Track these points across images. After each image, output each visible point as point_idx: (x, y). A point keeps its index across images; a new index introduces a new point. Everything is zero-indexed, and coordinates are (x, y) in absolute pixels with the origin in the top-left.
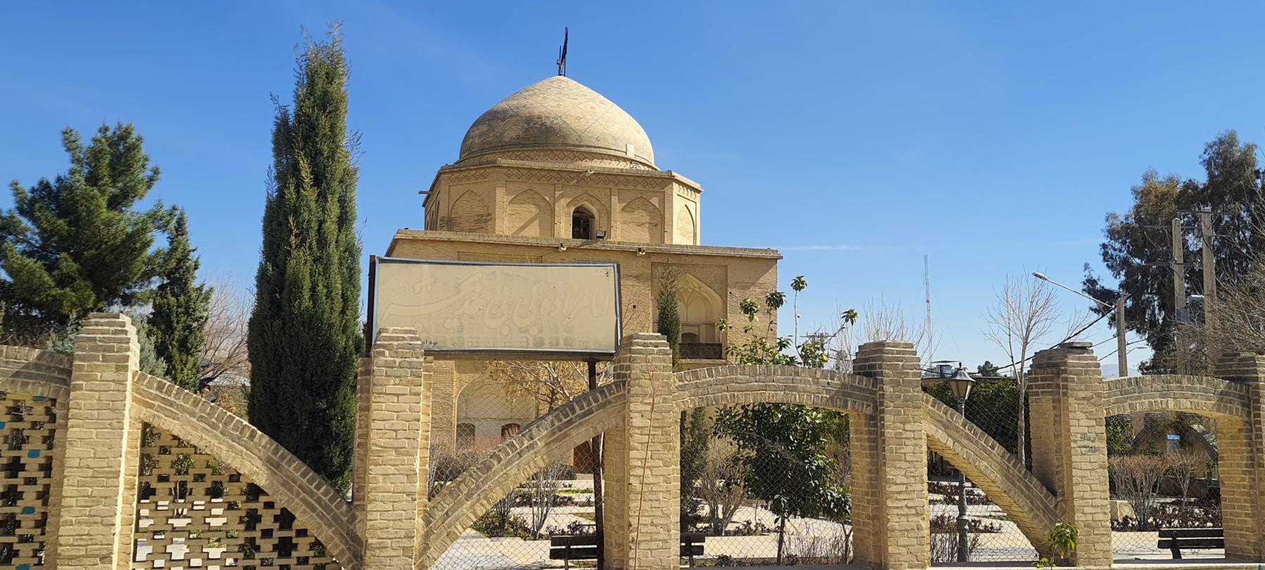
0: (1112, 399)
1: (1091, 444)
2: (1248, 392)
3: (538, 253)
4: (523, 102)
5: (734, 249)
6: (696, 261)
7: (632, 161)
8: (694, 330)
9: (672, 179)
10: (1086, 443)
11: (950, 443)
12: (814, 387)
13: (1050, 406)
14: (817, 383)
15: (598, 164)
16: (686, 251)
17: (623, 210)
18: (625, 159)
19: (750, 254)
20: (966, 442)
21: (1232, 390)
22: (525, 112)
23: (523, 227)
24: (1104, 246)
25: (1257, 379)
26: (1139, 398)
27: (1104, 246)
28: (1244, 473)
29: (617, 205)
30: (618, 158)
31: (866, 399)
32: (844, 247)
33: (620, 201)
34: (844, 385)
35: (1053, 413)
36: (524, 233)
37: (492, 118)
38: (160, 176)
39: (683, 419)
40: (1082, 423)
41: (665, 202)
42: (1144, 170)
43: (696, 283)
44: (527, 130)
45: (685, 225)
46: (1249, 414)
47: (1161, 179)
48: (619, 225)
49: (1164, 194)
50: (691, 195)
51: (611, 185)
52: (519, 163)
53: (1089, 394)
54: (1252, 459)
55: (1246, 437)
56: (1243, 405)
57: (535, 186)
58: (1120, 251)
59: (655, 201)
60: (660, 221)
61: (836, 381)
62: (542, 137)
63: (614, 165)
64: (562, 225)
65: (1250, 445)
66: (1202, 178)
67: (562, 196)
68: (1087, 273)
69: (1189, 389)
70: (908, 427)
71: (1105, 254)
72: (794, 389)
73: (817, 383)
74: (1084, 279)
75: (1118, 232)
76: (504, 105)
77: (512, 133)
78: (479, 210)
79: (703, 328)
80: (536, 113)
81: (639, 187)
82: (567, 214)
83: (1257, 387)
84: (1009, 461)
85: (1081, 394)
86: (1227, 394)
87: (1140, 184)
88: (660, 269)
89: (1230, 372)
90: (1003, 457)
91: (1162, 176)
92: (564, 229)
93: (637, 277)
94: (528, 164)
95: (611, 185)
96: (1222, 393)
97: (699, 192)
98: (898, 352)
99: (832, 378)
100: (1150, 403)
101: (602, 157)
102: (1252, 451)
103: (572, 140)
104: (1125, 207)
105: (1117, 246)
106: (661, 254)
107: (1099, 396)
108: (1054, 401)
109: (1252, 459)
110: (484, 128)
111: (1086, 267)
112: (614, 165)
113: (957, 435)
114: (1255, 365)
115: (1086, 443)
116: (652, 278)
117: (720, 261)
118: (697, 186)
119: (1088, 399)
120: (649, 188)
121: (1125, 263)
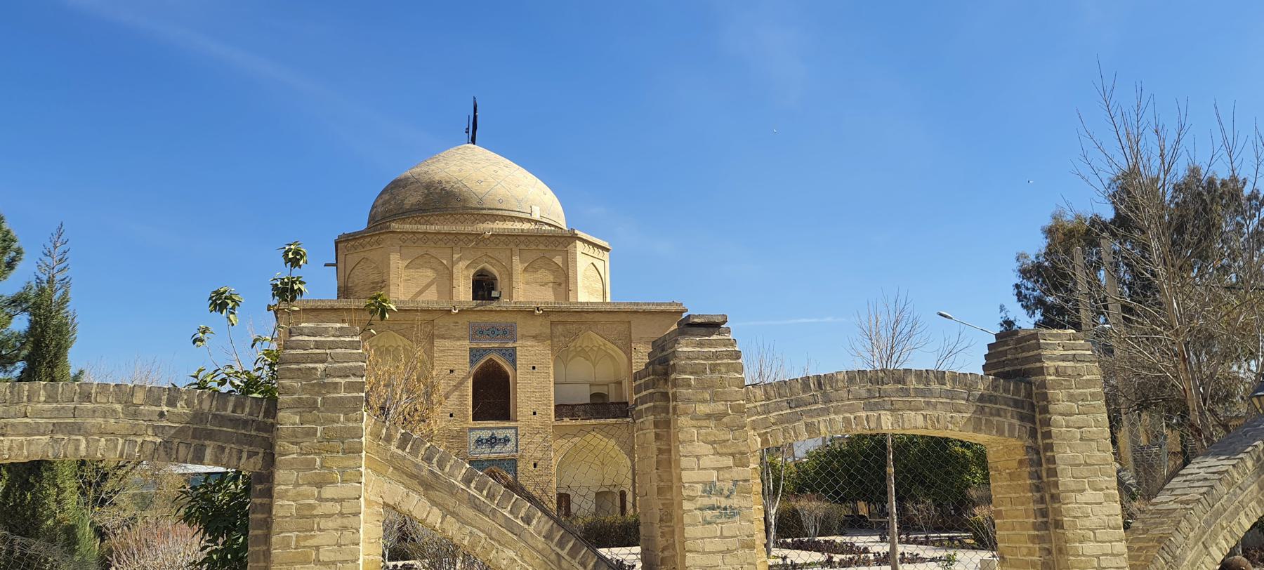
0: (772, 417)
1: (724, 502)
2: (1029, 395)
3: (428, 317)
4: (426, 169)
5: (637, 304)
6: (597, 317)
7: (536, 222)
8: (603, 390)
9: (575, 237)
10: (714, 500)
11: (435, 517)
12: (126, 423)
13: (651, 433)
14: (135, 415)
15: (499, 226)
16: (586, 308)
17: (525, 270)
18: (529, 221)
19: (653, 308)
20: (469, 513)
21: (1000, 393)
22: (425, 178)
23: (420, 292)
24: (1017, 286)
25: (1041, 371)
26: (826, 411)
27: (1017, 286)
28: (1033, 539)
29: (518, 266)
30: (521, 220)
31: (250, 440)
32: (829, 319)
33: (522, 261)
34: (198, 416)
35: (654, 446)
36: (419, 299)
37: (397, 185)
38: (23, 256)
39: (986, 477)
40: (705, 462)
41: (569, 260)
42: (1052, 209)
43: (600, 341)
44: (427, 195)
45: (591, 281)
46: (1033, 434)
47: (1069, 218)
48: (521, 286)
49: (1071, 231)
50: (597, 253)
51: (512, 246)
52: (414, 227)
53: (720, 407)
54: (1044, 513)
55: (1031, 475)
56: (1022, 418)
57: (425, 249)
58: (1034, 290)
59: (558, 260)
60: (564, 280)
61: (181, 408)
62: (443, 202)
63: (518, 226)
64: (461, 288)
65: (1038, 489)
66: (1108, 214)
67: (460, 259)
68: (1003, 314)
69: (920, 393)
70: (328, 492)
71: (1019, 294)
72: (77, 429)
73: (135, 415)
74: (1001, 321)
75: (1029, 271)
76: (408, 174)
77: (412, 199)
78: (374, 277)
79: (612, 386)
80: (437, 178)
81: (542, 247)
82: (466, 277)
83: (1043, 385)
84: (561, 544)
85: (703, 409)
86: (992, 399)
87: (1048, 222)
88: (560, 328)
89: (1003, 364)
90: (548, 537)
91: (1069, 217)
92: (463, 292)
93: (535, 337)
94: (422, 228)
95: (512, 246)
96: (982, 398)
97: (608, 250)
98: (318, 345)
99: (171, 403)
100: (847, 420)
101: (504, 218)
102: (1042, 500)
103: (474, 203)
104: (1035, 246)
105: (1030, 285)
106: (561, 312)
107: (739, 410)
108: (656, 425)
109: (1044, 513)
110: (387, 197)
111: (1002, 308)
112: (518, 226)
113: (451, 502)
114: (1039, 346)
115: (714, 500)
116: (552, 337)
117: (623, 317)
118: (605, 244)
119: (718, 417)
120: (551, 247)
121: (1040, 302)
